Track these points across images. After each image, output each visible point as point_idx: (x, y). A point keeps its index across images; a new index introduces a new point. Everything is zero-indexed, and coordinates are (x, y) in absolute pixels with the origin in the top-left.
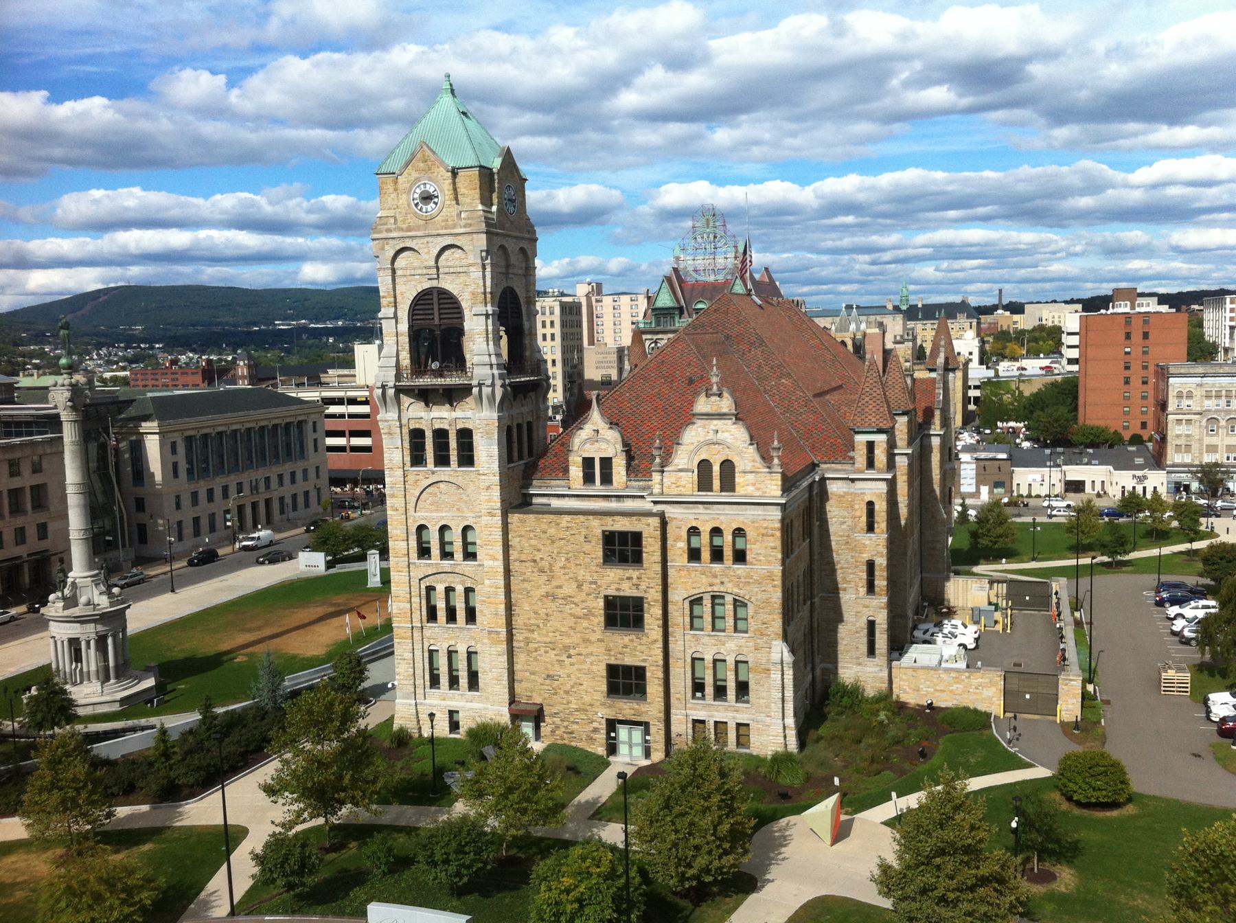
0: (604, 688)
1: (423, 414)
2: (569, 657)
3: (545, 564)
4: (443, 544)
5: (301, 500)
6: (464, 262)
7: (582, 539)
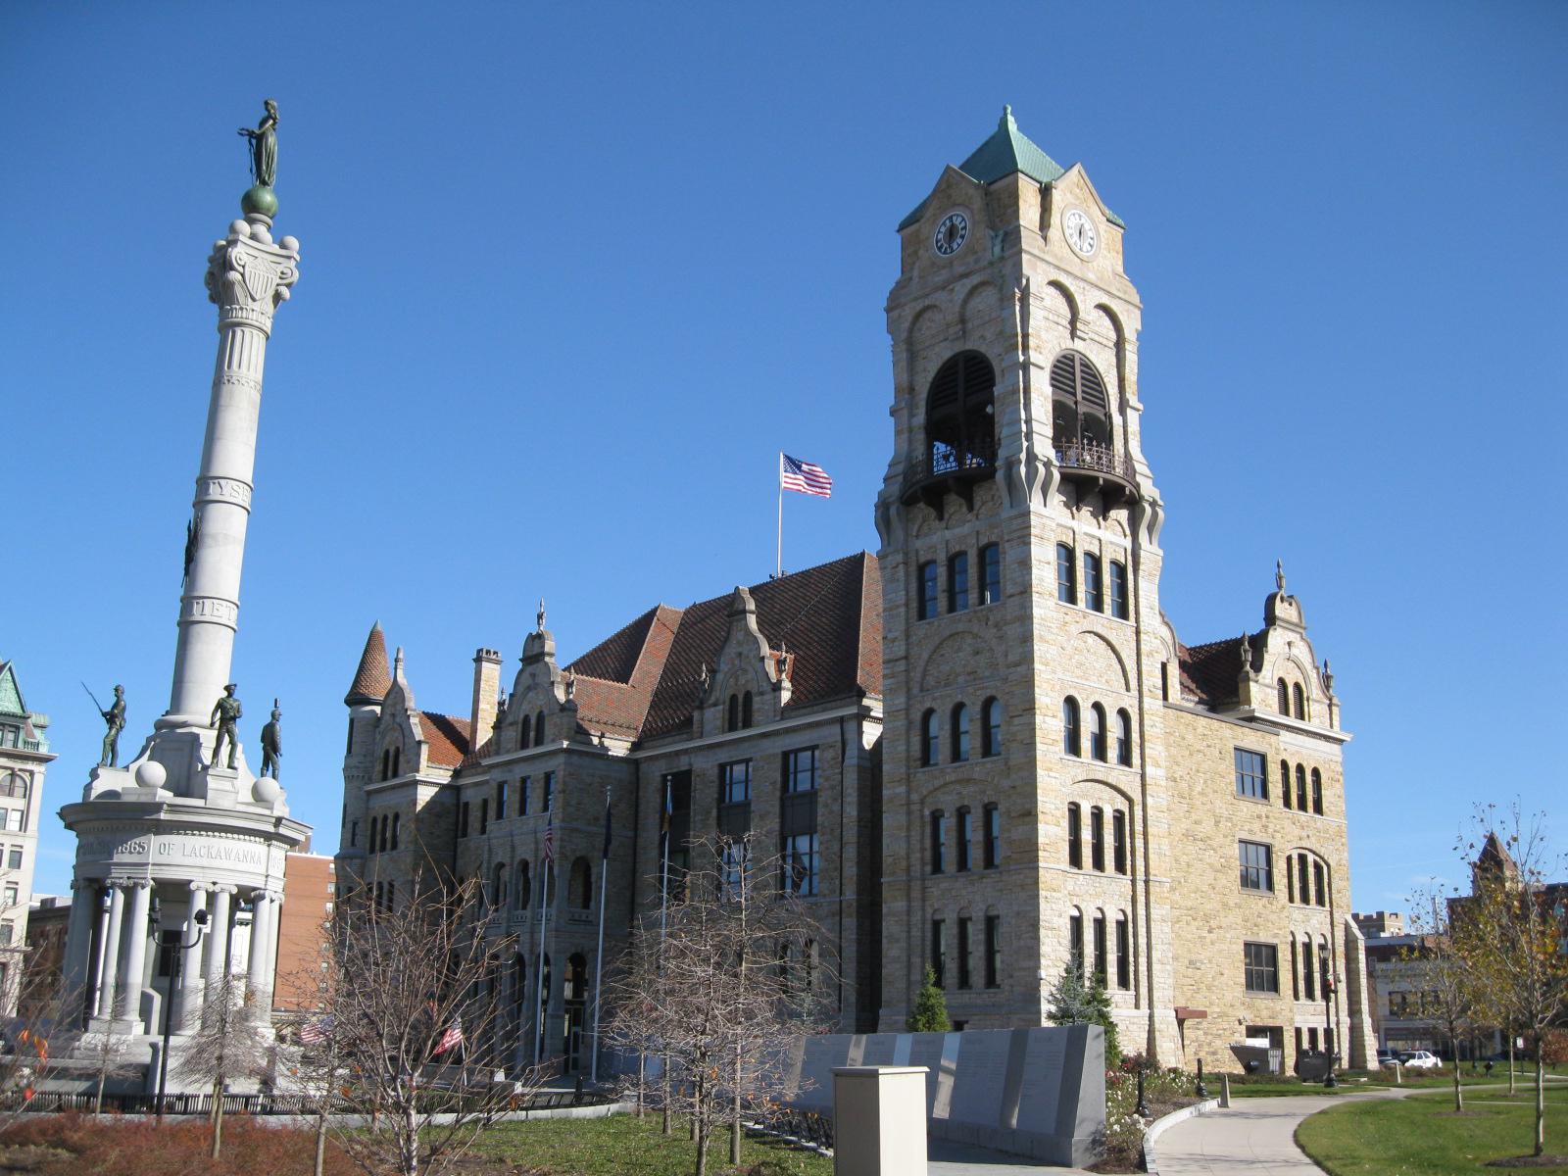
5: (511, 797)
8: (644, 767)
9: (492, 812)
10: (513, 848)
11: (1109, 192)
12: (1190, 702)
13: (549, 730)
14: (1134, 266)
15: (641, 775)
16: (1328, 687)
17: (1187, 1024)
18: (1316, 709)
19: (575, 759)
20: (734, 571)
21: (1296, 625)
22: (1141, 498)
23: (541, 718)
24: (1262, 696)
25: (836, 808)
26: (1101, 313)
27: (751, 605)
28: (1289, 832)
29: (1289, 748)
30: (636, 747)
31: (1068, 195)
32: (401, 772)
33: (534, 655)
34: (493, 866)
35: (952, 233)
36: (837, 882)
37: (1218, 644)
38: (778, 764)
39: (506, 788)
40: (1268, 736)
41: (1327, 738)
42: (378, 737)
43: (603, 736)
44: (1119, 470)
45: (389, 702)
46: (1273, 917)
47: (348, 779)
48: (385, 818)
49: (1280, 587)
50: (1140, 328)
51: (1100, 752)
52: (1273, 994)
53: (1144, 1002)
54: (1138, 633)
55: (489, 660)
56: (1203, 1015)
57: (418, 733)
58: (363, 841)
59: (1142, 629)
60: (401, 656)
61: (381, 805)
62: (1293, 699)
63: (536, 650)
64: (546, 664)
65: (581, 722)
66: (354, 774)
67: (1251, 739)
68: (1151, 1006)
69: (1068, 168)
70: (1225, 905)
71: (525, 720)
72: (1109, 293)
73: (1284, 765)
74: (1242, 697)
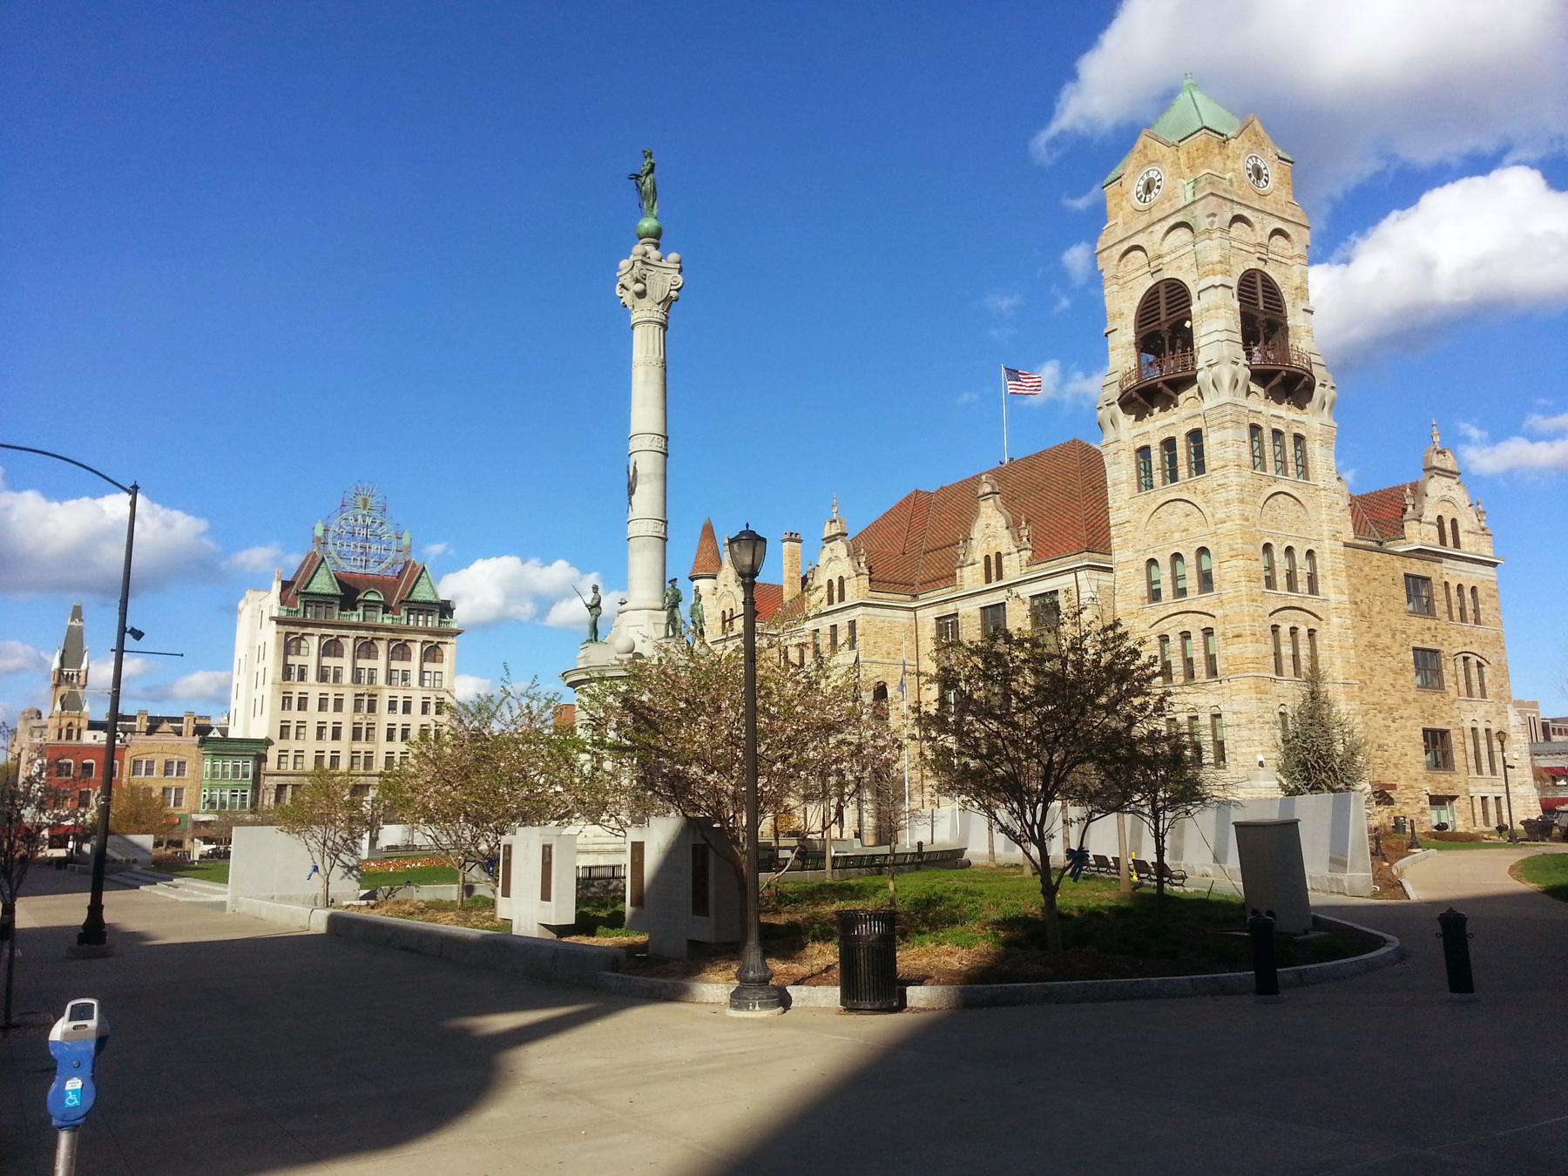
1: (1261, 408)
3: (1364, 607)
4: (1176, 578)
6: (1289, 253)
35: (1148, 188)
46: (1446, 708)
51: (1292, 585)
70: (1405, 700)
72: (1283, 219)
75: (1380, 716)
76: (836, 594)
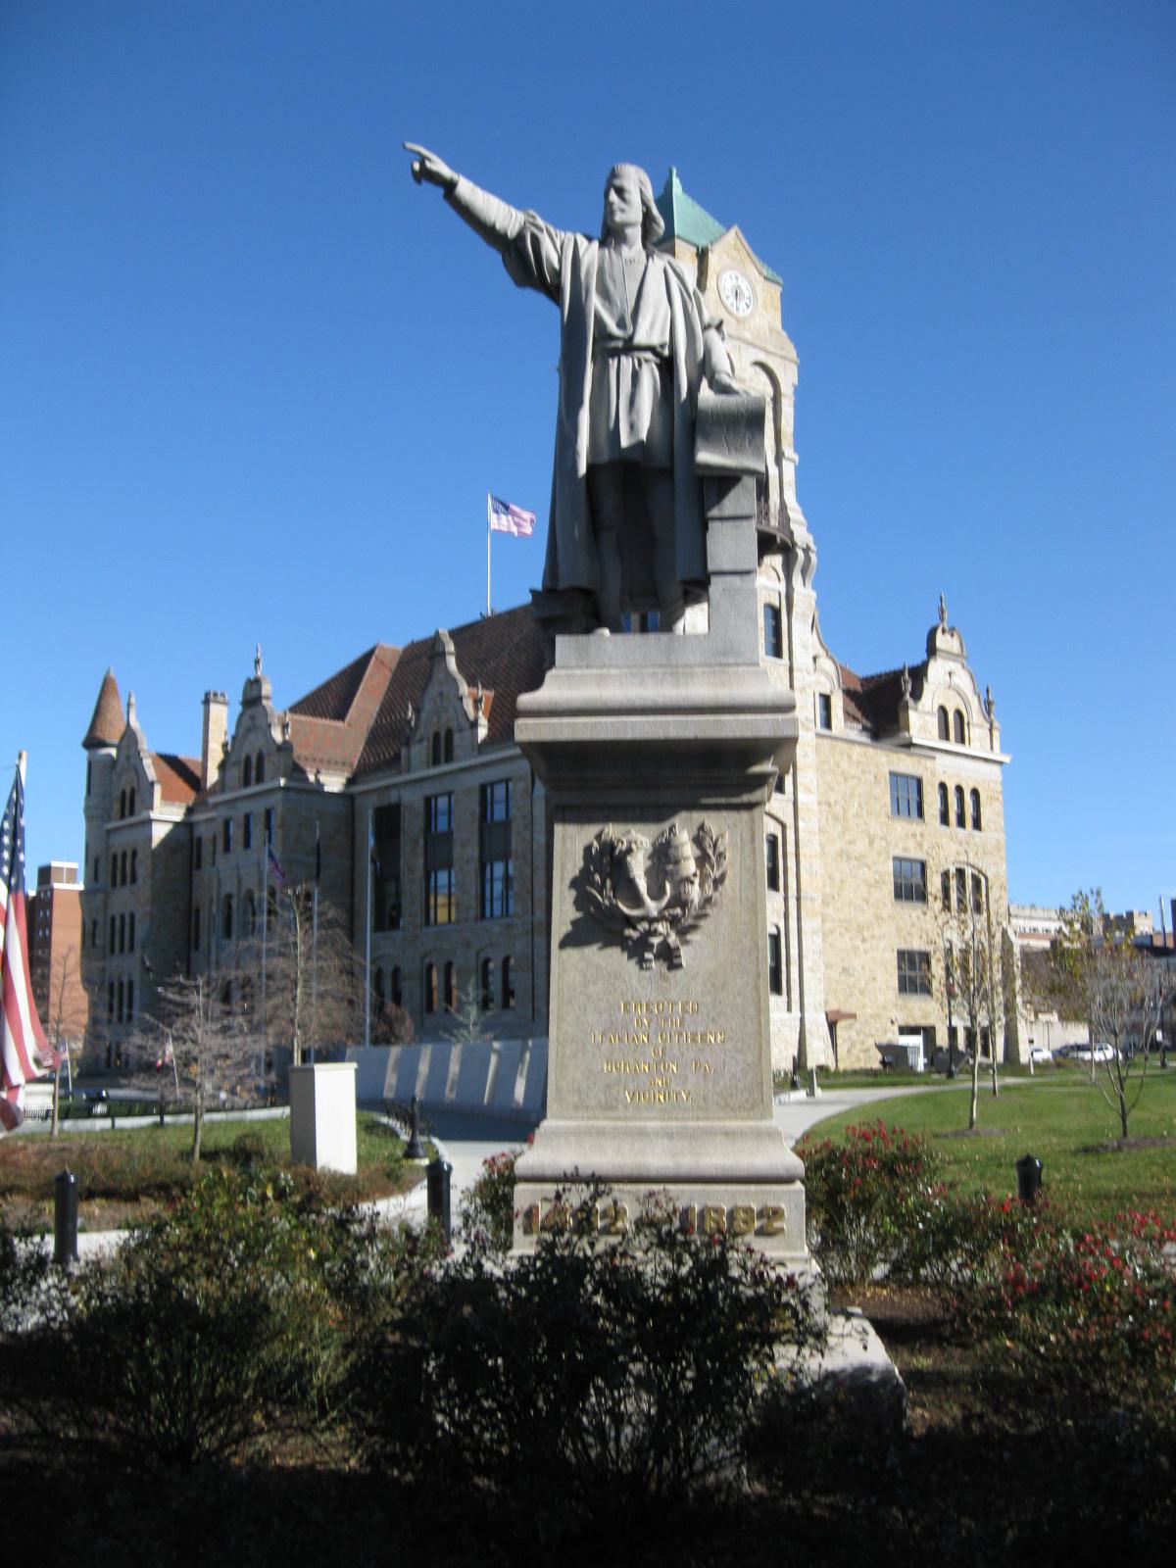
0: (895, 983)
2: (864, 940)
3: (838, 809)
5: (237, 833)
7: (872, 778)
8: (358, 801)
9: (220, 847)
10: (240, 880)
11: (765, 248)
12: (854, 732)
13: (268, 768)
14: (794, 320)
15: (356, 809)
16: (989, 713)
17: (840, 1025)
18: (977, 732)
19: (293, 795)
20: (440, 618)
21: (957, 655)
22: (794, 544)
23: (261, 758)
24: (921, 723)
25: (527, 835)
26: (759, 370)
27: (450, 647)
28: (943, 848)
29: (945, 769)
30: (350, 782)
31: (725, 256)
32: (137, 809)
33: (252, 699)
34: (222, 896)
36: (530, 903)
37: (887, 674)
38: (476, 796)
39: (232, 824)
40: (923, 761)
41: (986, 760)
42: (114, 778)
43: (318, 772)
44: (774, 522)
45: (124, 744)
47: (89, 818)
48: (124, 855)
49: (942, 620)
50: (796, 383)
52: (926, 997)
53: (796, 1006)
54: (791, 670)
55: (217, 702)
56: (853, 1016)
57: (151, 773)
58: (105, 876)
59: (795, 665)
60: (133, 700)
61: (119, 843)
62: (952, 725)
63: (254, 693)
64: (264, 708)
65: (297, 761)
66: (95, 814)
67: (906, 764)
68: (802, 1009)
69: (728, 229)
70: (879, 918)
71: (251, 758)
73: (943, 787)
74: (902, 724)
75: (847, 936)
76: (253, 774)
